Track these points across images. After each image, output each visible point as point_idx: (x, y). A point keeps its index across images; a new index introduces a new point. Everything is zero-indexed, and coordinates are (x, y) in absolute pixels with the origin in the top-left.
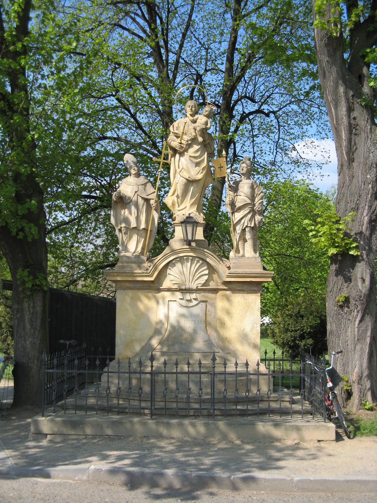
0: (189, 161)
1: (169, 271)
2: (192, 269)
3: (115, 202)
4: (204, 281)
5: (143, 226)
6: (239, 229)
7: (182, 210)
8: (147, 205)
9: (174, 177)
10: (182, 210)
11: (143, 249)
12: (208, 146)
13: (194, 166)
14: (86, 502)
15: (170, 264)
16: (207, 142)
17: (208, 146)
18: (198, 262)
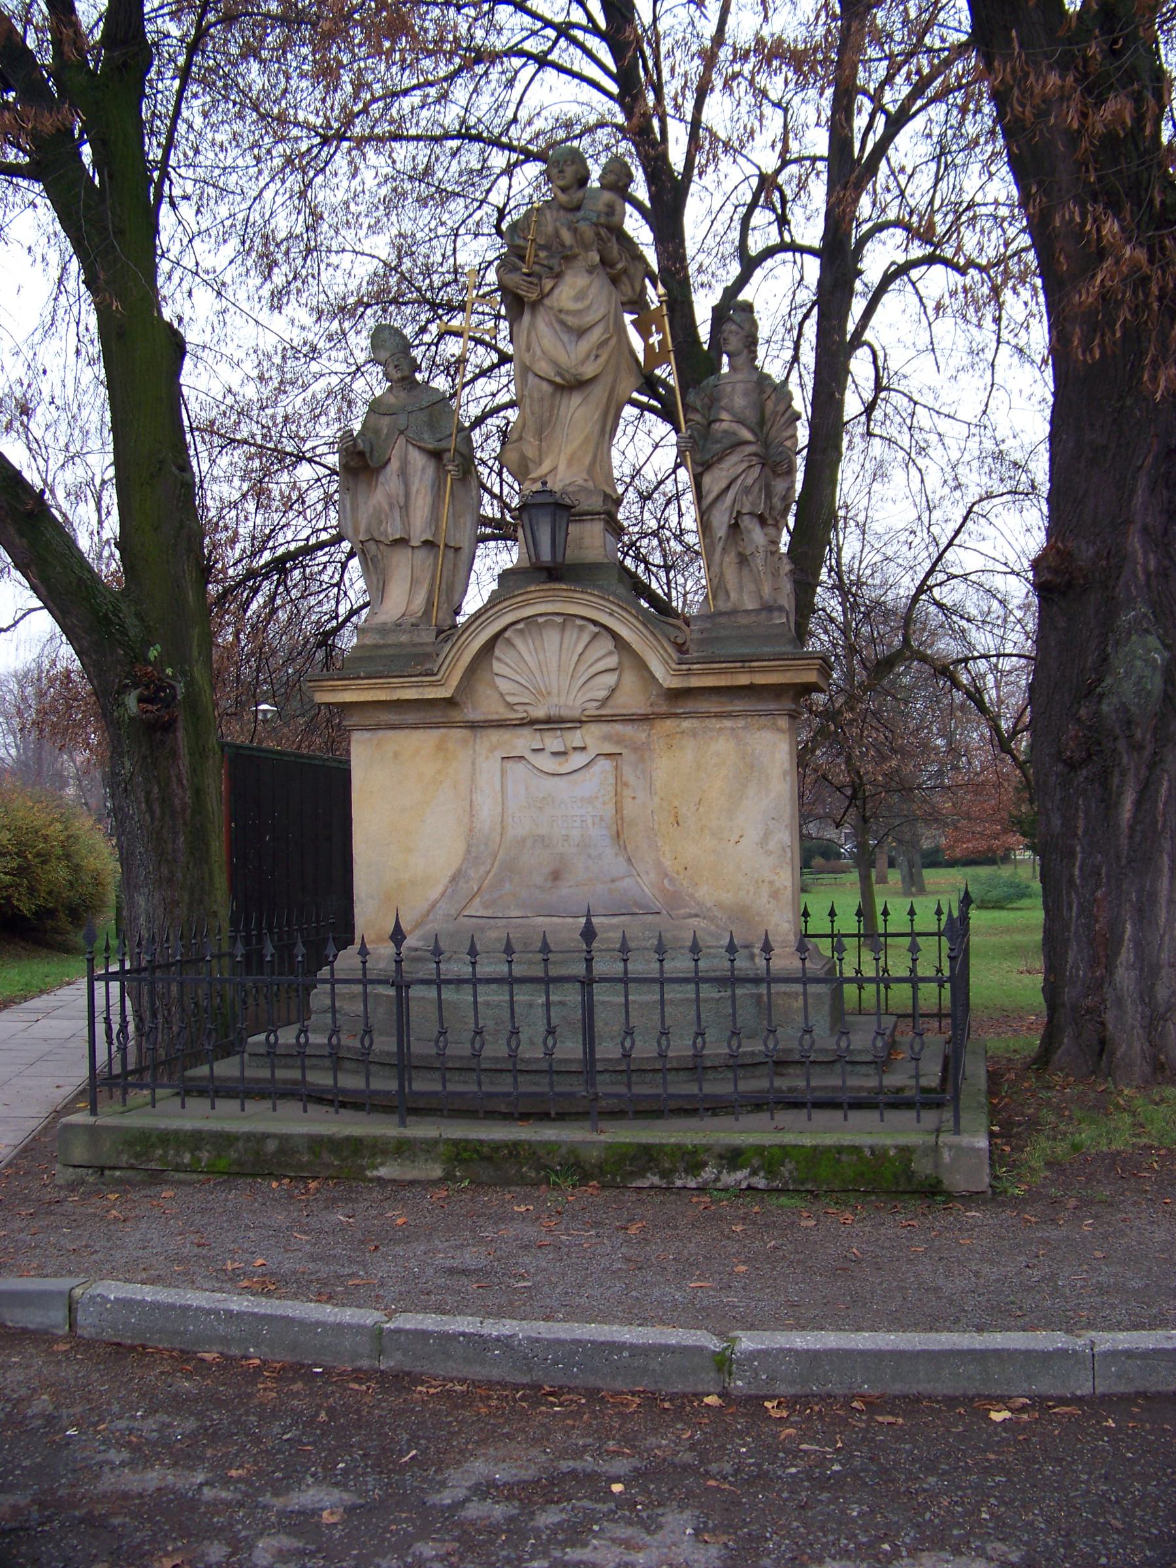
1: (497, 667)
5: (419, 531)
12: (625, 279)
16: (620, 266)
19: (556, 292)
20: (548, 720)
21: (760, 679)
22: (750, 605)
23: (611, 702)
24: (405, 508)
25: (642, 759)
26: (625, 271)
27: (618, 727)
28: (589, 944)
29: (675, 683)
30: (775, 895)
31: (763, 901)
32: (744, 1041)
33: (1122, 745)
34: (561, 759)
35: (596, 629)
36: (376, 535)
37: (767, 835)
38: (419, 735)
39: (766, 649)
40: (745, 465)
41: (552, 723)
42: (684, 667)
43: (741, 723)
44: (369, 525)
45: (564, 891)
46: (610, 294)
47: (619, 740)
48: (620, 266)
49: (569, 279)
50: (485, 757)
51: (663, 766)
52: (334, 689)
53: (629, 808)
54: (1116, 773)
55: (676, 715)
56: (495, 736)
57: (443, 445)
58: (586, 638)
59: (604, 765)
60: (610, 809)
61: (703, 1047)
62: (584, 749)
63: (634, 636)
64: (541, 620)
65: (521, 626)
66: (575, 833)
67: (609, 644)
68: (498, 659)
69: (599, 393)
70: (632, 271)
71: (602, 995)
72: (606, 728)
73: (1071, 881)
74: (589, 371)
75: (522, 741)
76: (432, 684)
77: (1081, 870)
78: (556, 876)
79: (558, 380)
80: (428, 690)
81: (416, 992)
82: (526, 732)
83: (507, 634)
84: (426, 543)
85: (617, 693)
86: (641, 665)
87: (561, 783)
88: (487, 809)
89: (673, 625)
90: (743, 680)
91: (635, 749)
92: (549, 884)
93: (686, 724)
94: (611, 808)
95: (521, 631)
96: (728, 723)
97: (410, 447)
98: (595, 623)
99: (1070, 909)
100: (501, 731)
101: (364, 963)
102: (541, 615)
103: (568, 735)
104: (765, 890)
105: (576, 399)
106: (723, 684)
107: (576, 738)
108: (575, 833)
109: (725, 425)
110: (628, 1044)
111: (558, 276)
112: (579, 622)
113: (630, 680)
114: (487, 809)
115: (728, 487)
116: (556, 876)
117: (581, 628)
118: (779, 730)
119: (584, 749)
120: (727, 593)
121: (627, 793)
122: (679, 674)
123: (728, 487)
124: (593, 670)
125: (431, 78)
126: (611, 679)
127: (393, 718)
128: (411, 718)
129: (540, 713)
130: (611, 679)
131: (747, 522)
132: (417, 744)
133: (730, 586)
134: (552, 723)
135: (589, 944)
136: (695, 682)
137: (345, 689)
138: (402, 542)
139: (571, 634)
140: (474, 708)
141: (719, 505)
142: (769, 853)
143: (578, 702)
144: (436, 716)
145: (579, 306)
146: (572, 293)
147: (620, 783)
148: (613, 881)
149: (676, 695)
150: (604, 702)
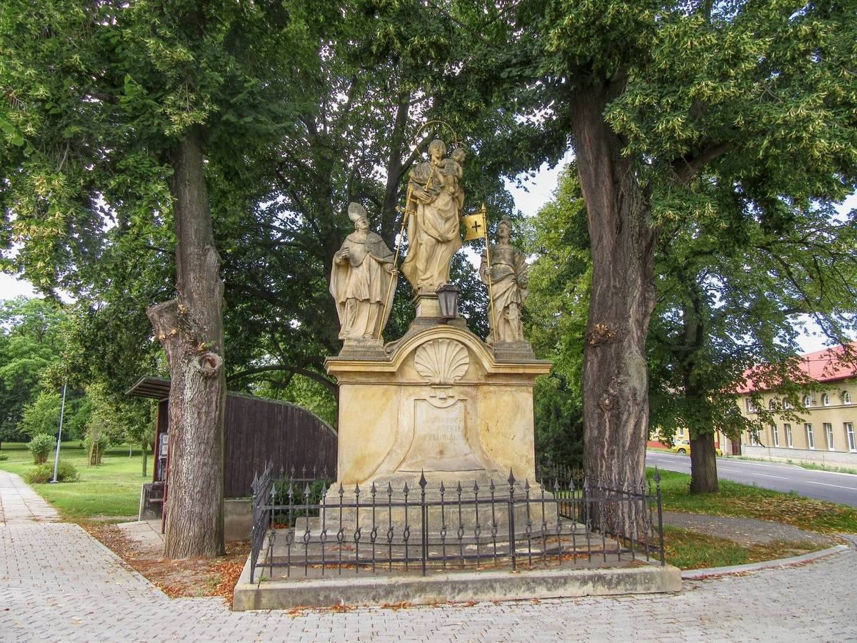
1: (417, 359)
2: (447, 359)
6: (500, 305)
19: (437, 201)
20: (440, 384)
21: (528, 371)
22: (508, 340)
25: (474, 402)
27: (466, 388)
28: (512, 484)
30: (528, 462)
31: (523, 465)
32: (466, 532)
33: (630, 403)
34: (443, 401)
37: (525, 436)
38: (375, 388)
41: (442, 385)
43: (514, 389)
45: (446, 460)
47: (466, 394)
49: (442, 196)
50: (405, 399)
51: (481, 406)
53: (470, 424)
54: (626, 413)
55: (489, 384)
56: (411, 389)
58: (458, 349)
59: (461, 404)
60: (462, 424)
61: (463, 534)
62: (453, 397)
64: (440, 340)
66: (449, 434)
67: (466, 353)
69: (451, 245)
71: (434, 511)
72: (461, 388)
73: (603, 455)
75: (425, 392)
76: (388, 365)
77: (607, 451)
78: (441, 453)
81: (431, 510)
82: (428, 388)
84: (378, 302)
87: (443, 411)
88: (406, 423)
90: (521, 371)
91: (472, 398)
92: (438, 457)
93: (492, 388)
94: (463, 423)
95: (431, 345)
96: (509, 389)
98: (462, 343)
99: (602, 466)
100: (414, 388)
101: (341, 497)
103: (447, 391)
104: (524, 460)
105: (444, 247)
107: (451, 392)
108: (449, 434)
110: (443, 533)
111: (438, 195)
112: (456, 342)
113: (472, 368)
114: (406, 423)
116: (441, 453)
117: (457, 345)
118: (529, 392)
119: (453, 397)
121: (469, 416)
124: (460, 363)
126: (466, 367)
127: (364, 379)
128: (372, 380)
129: (437, 381)
131: (513, 307)
132: (375, 392)
134: (442, 385)
135: (512, 484)
136: (501, 371)
139: (452, 348)
140: (402, 377)
141: (500, 298)
142: (525, 444)
144: (384, 379)
147: (466, 413)
148: (466, 455)
149: (490, 375)
150: (462, 377)
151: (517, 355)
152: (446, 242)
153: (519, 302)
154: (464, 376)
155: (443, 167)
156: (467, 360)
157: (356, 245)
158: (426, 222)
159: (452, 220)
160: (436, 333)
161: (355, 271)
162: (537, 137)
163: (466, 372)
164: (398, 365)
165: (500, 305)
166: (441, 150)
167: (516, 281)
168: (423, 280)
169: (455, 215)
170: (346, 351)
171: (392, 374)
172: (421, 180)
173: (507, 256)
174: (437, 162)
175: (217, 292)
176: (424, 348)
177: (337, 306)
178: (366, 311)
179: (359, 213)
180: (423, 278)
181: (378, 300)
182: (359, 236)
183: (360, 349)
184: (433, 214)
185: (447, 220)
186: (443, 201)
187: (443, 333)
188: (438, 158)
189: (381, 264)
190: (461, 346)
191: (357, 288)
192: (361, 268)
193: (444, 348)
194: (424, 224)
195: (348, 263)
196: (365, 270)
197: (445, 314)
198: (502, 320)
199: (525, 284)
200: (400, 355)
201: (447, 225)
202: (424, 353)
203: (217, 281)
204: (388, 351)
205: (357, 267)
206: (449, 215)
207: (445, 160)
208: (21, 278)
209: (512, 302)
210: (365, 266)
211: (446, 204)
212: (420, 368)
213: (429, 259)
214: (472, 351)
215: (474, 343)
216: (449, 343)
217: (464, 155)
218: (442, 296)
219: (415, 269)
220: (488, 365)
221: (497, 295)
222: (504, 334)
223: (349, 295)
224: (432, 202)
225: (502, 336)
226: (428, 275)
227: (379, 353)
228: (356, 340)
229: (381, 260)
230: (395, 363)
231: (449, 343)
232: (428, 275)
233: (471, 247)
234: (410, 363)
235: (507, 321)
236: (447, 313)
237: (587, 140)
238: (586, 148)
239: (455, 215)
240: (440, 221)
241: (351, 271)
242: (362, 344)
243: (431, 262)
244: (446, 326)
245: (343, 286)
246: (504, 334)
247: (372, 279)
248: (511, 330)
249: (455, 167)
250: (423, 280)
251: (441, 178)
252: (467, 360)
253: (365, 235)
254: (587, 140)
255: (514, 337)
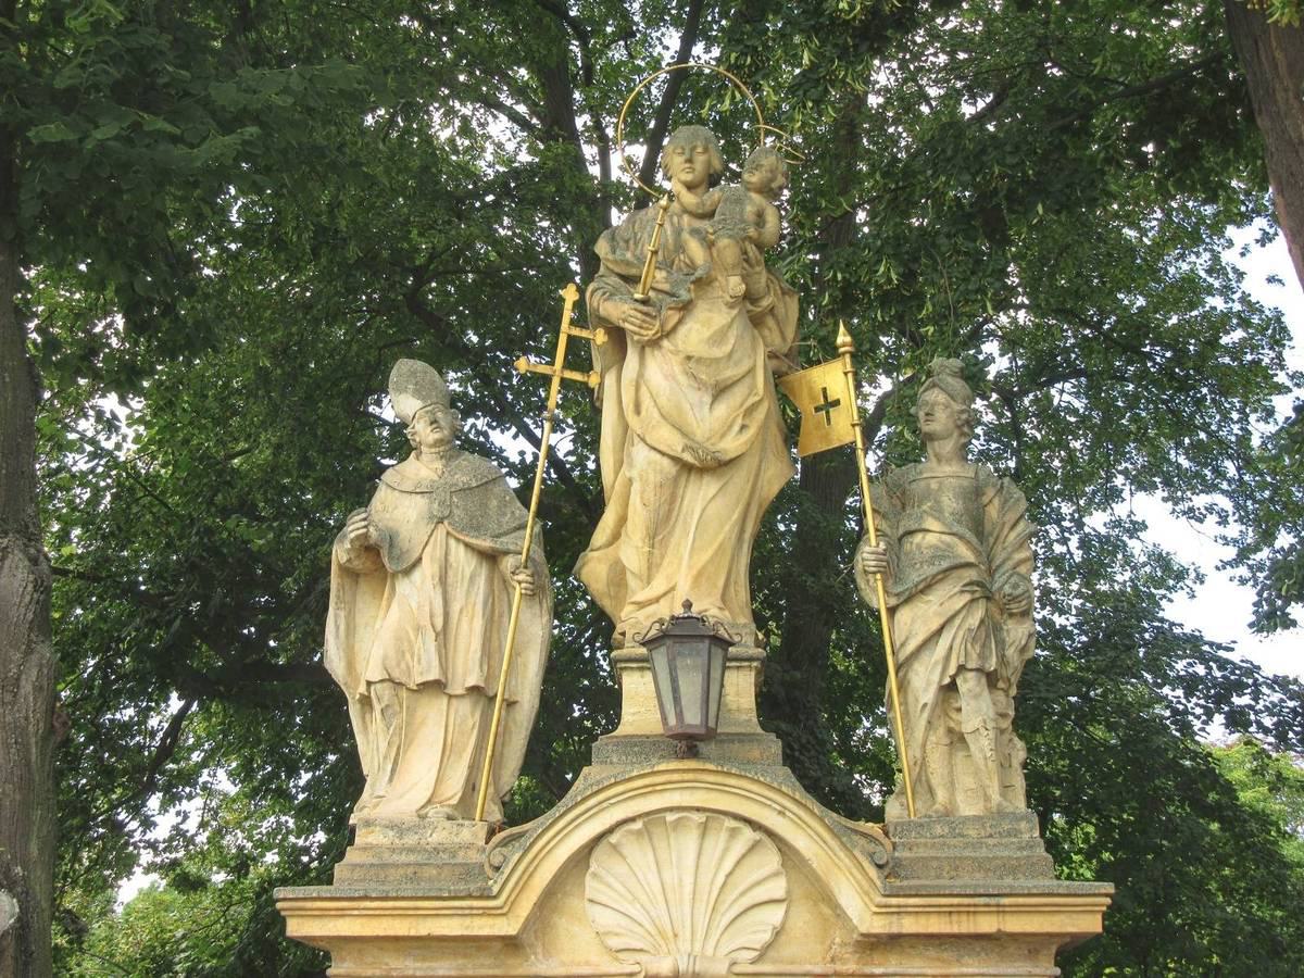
0: (682, 379)
1: (591, 886)
2: (704, 881)
3: (344, 569)
4: (767, 937)
5: (468, 673)
6: (925, 680)
7: (657, 600)
8: (490, 581)
9: (619, 464)
10: (657, 600)
11: (471, 787)
12: (770, 322)
13: (707, 399)
14: (665, 967)
15: (600, 853)
16: (765, 303)
17: (770, 322)
18: (716, 841)
19: (682, 330)
21: (1014, 925)
23: (772, 954)
24: (444, 636)
26: (772, 310)
29: (879, 926)
35: (757, 836)
36: (396, 675)
39: (1030, 883)
40: (967, 597)
42: (894, 901)
44: (385, 658)
46: (754, 338)
48: (765, 303)
52: (323, 915)
57: (506, 542)
63: (815, 848)
64: (670, 817)
65: (638, 825)
67: (770, 859)
68: (595, 875)
70: (780, 310)
74: (731, 445)
76: (486, 913)
79: (688, 457)
80: (478, 921)
83: (613, 839)
85: (783, 938)
86: (823, 896)
89: (865, 835)
90: (987, 924)
95: (639, 833)
97: (452, 542)
102: (671, 809)
106: (955, 929)
109: (931, 539)
111: (686, 308)
112: (730, 823)
113: (803, 919)
115: (939, 632)
117: (733, 832)
120: (931, 791)
122: (885, 911)
123: (939, 632)
125: (1137, 98)
126: (776, 915)
130: (776, 915)
131: (967, 684)
133: (935, 781)
136: (909, 925)
137: (341, 914)
138: (437, 686)
140: (547, 954)
143: (724, 949)
145: (718, 352)
146: (707, 333)
150: (764, 953)
151: (981, 865)
152: (717, 466)
153: (992, 664)
154: (768, 946)
155: (710, 215)
156: (778, 888)
157: (408, 500)
158: (646, 403)
159: (738, 393)
160: (652, 790)
161: (403, 586)
162: (1163, 85)
163: (778, 933)
164: (525, 907)
165: (925, 680)
166: (700, 160)
167: (983, 591)
168: (641, 605)
169: (751, 371)
170: (355, 866)
171: (511, 944)
172: (628, 264)
173: (950, 503)
174: (689, 199)
175: (27, 687)
176: (615, 847)
177: (354, 711)
178: (434, 718)
179: (417, 393)
180: (641, 596)
181: (472, 681)
182: (421, 469)
183: (403, 858)
184: (670, 377)
185: (720, 391)
186: (707, 327)
187: (682, 788)
188: (690, 187)
189: (491, 558)
190: (748, 835)
191: (403, 647)
192: (417, 575)
193: (689, 841)
194: (638, 411)
195: (381, 563)
196: (429, 584)
197: (672, 721)
198: (939, 736)
199: (1014, 599)
200: (529, 875)
201: (722, 409)
202: (620, 868)
203: (29, 651)
204: (496, 861)
205: (407, 572)
206: (730, 373)
207: (715, 193)
208: (365, 728)
209: (961, 668)
210: (427, 572)
211: (719, 337)
212: (604, 918)
213: (660, 529)
214: (796, 852)
215: (800, 823)
216: (704, 829)
217: (783, 167)
218: (660, 658)
219: (619, 575)
220: (860, 905)
221: (439, 611)
222: (951, 786)
223: (374, 673)
224: (668, 334)
225: (941, 795)
226: (658, 586)
227: (470, 872)
228: (392, 826)
229: (486, 543)
230: (513, 903)
231: (704, 829)
232: (658, 586)
233: (1160, 493)
234: (574, 903)
235: (957, 739)
236: (680, 715)
237: (1283, 70)
238: (1280, 96)
239: (751, 371)
240: (694, 396)
241: (393, 588)
242: (411, 840)
243: (665, 543)
244: (692, 764)
245: (367, 641)
246: (951, 786)
247: (454, 616)
248: (977, 773)
249: (749, 209)
250: (641, 605)
251: (696, 250)
252: (778, 888)
253: (439, 465)
254: (1283, 70)
255: (987, 798)
